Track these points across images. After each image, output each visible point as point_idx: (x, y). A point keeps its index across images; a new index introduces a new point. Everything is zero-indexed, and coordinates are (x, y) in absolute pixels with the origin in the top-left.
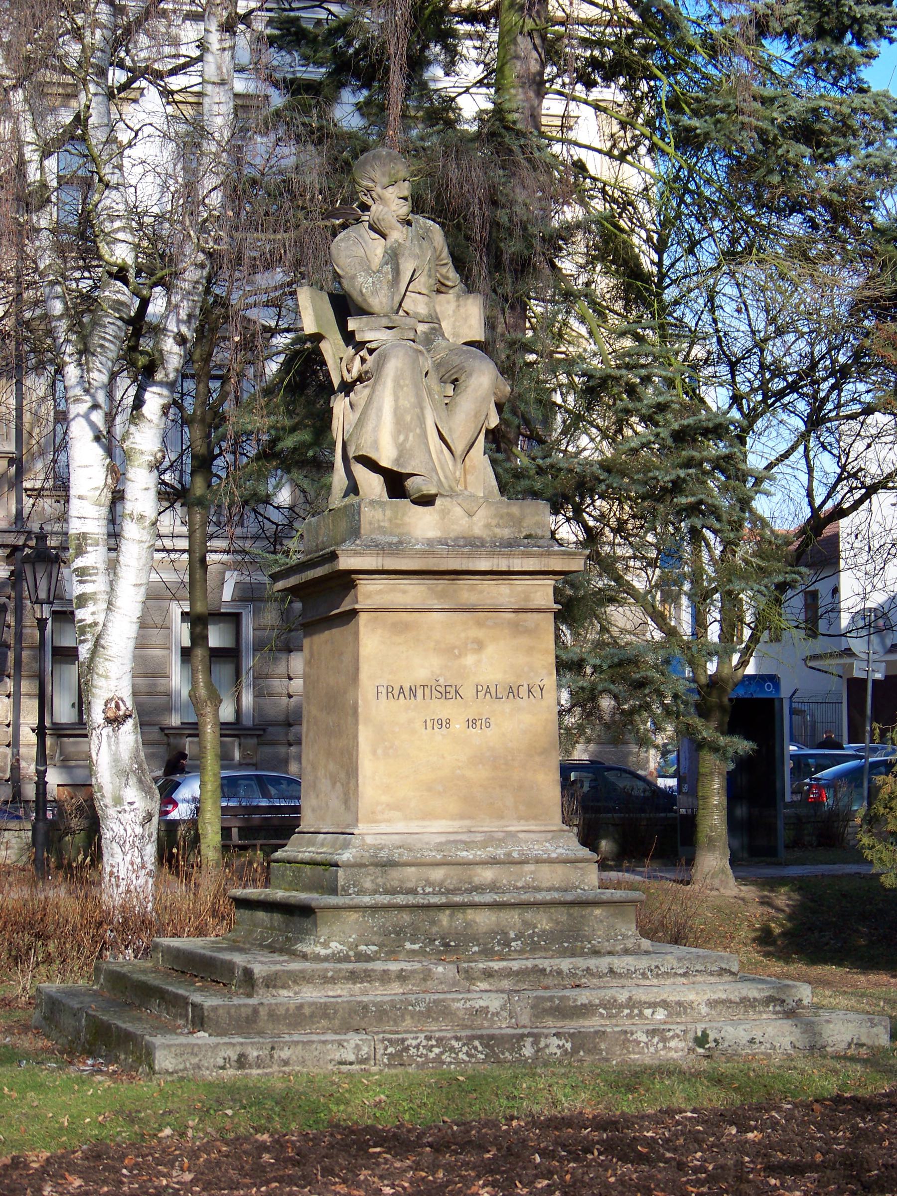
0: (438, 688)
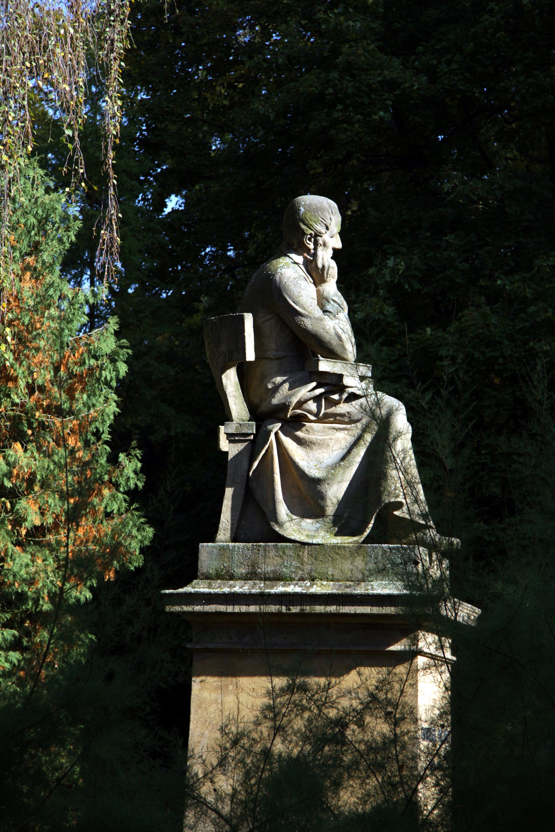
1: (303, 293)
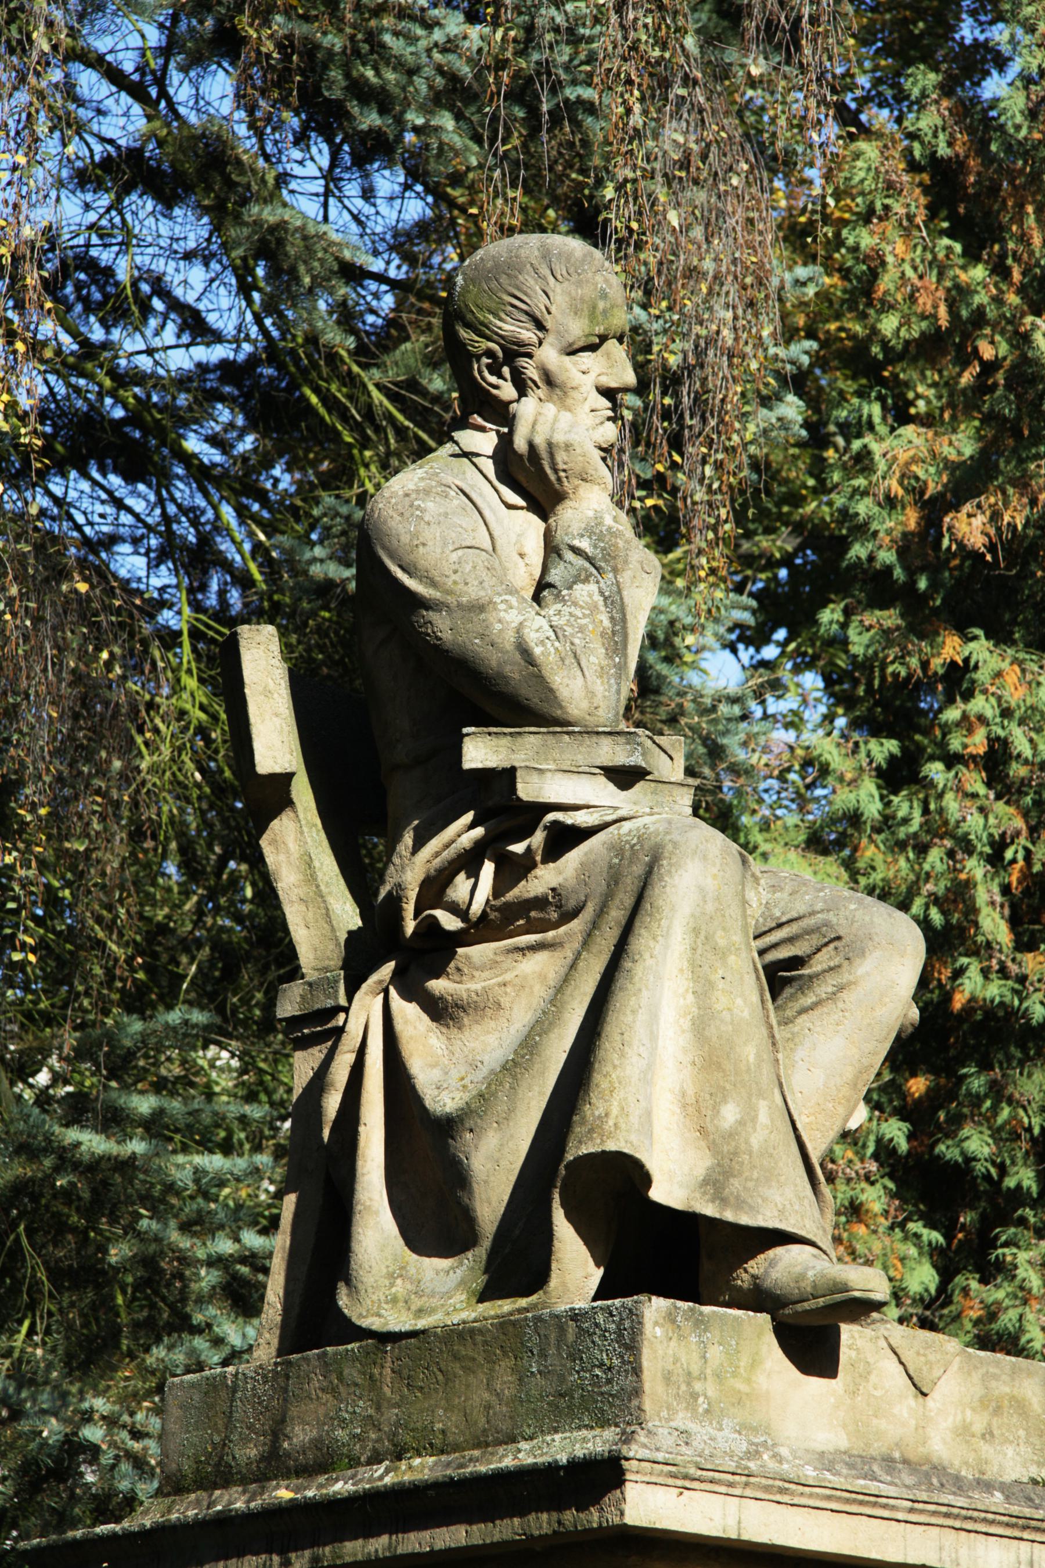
1: (431, 535)
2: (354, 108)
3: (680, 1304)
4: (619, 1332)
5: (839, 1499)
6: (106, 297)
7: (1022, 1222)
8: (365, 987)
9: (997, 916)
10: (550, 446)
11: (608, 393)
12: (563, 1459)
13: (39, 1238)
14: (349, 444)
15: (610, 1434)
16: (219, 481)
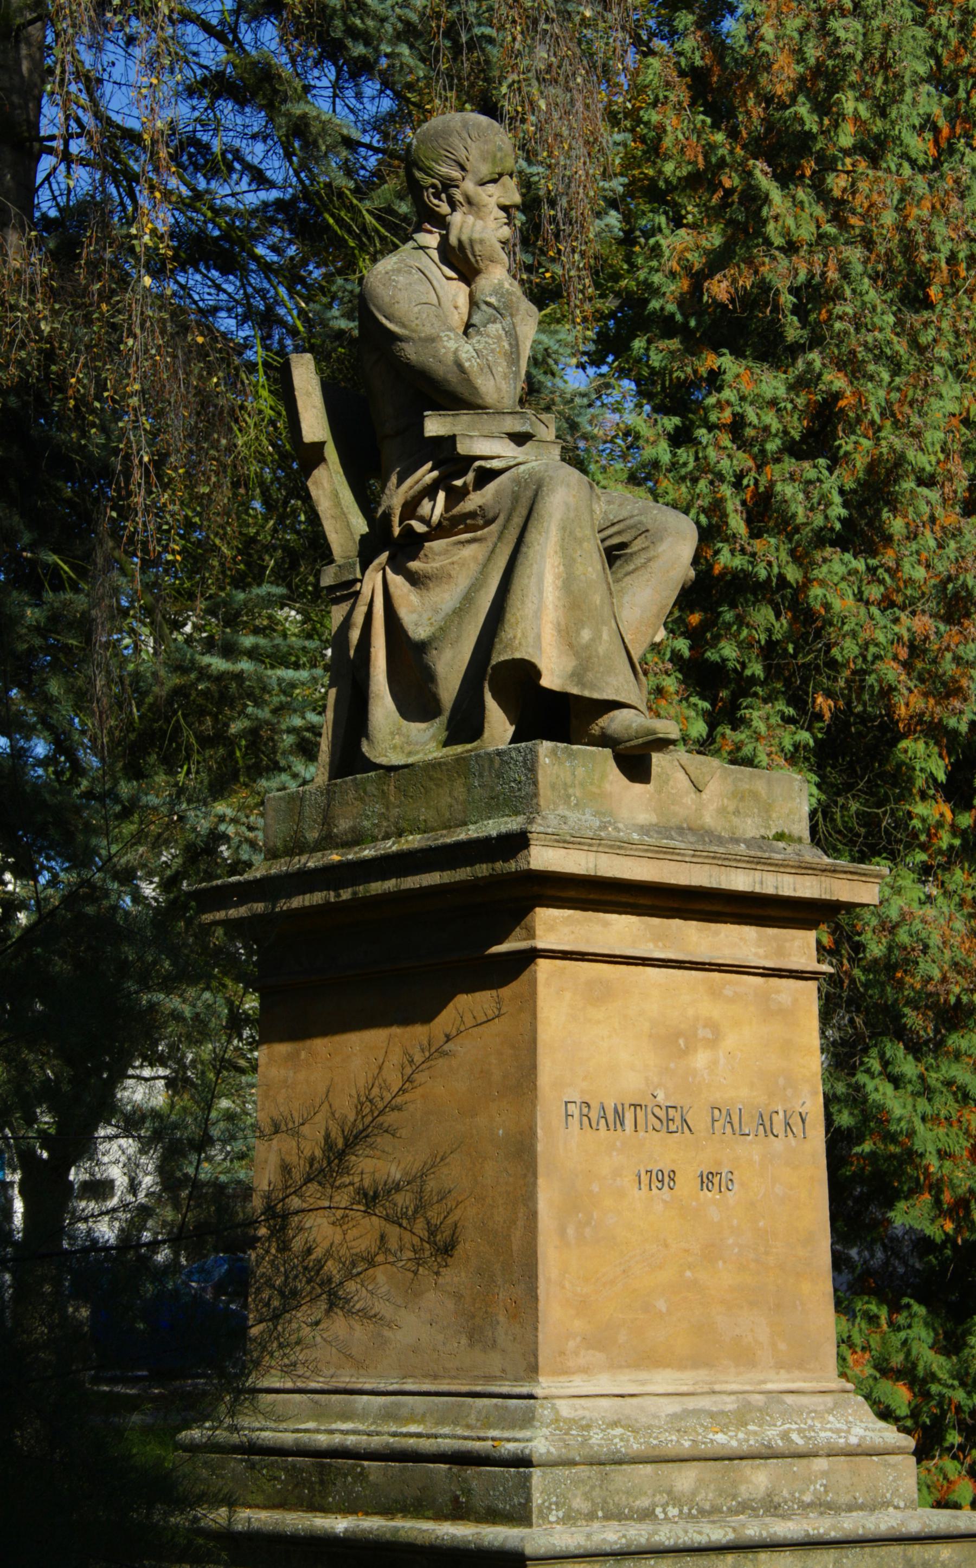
0: (657, 1111)
2: (349, 43)
3: (559, 744)
4: (525, 762)
5: (652, 851)
6: (207, 161)
7: (755, 695)
8: (371, 567)
9: (738, 518)
10: (471, 241)
11: (504, 208)
12: (494, 833)
13: (190, 719)
14: (353, 248)
15: (521, 819)
16: (276, 273)
